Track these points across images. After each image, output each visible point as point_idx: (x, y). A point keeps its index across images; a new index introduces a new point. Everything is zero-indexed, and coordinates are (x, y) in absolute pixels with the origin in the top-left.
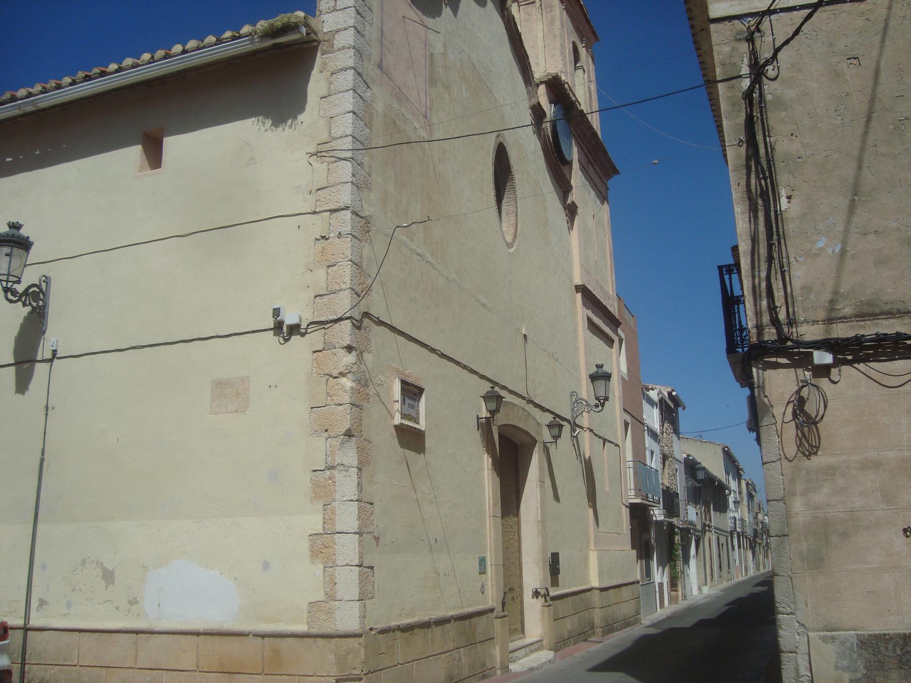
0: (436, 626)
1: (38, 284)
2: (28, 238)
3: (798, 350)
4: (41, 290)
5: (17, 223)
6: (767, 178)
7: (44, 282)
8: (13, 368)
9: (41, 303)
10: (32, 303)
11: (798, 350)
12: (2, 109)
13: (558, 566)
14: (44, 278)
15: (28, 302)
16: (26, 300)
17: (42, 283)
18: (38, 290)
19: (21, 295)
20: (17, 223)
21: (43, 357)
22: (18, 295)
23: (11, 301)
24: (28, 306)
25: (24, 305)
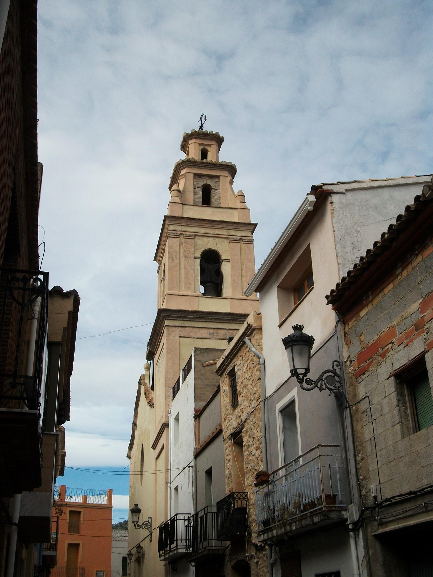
0: (228, 342)
1: (332, 369)
2: (312, 336)
3: (330, 505)
4: (336, 374)
5: (297, 325)
6: (188, 546)
7: (337, 366)
8: (184, 541)
9: (338, 385)
10: (328, 386)
11: (330, 505)
12: (427, 510)
13: (17, 216)
14: (335, 363)
15: (324, 387)
16: (321, 385)
17: (335, 367)
18: (333, 375)
19: (316, 382)
20: (297, 325)
21: (282, 465)
22: (313, 383)
23: (307, 390)
24: (324, 389)
25: (321, 389)
